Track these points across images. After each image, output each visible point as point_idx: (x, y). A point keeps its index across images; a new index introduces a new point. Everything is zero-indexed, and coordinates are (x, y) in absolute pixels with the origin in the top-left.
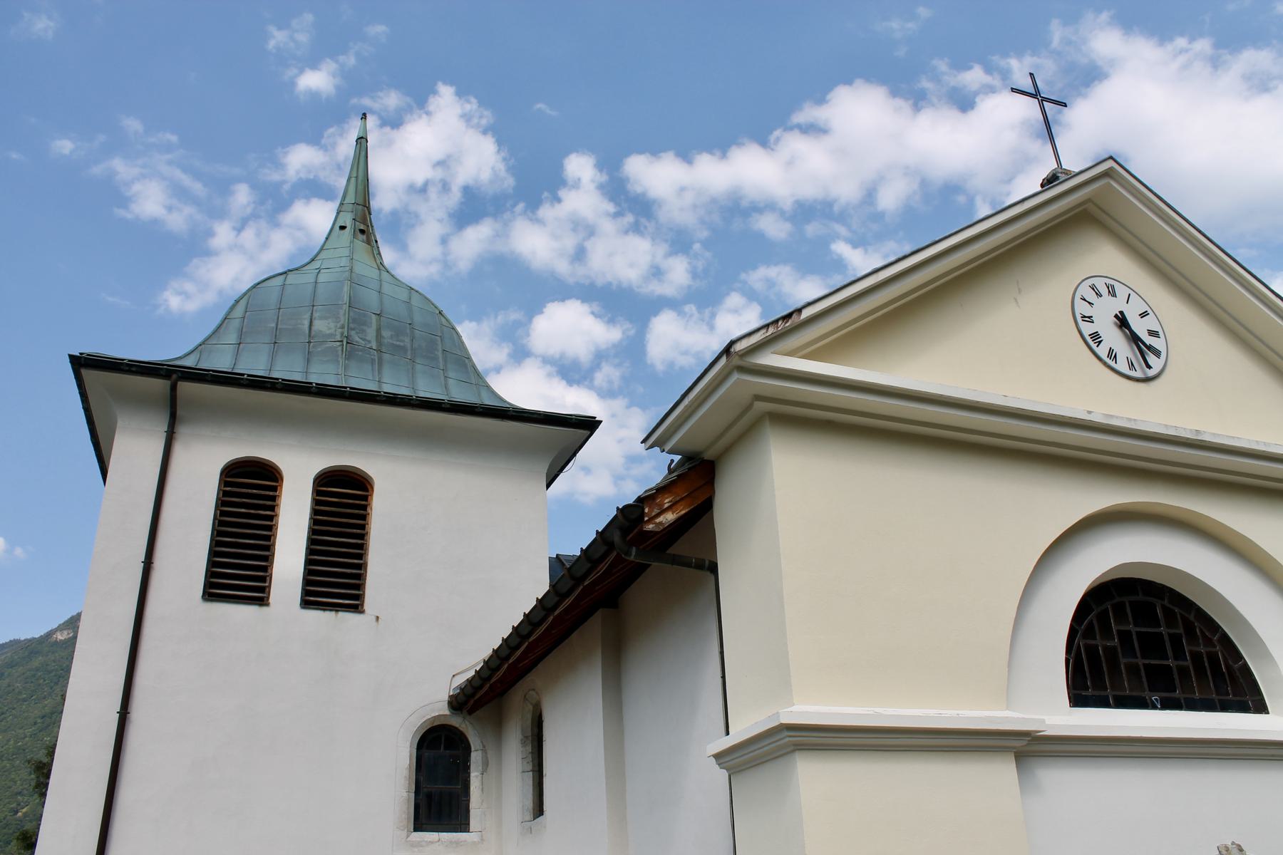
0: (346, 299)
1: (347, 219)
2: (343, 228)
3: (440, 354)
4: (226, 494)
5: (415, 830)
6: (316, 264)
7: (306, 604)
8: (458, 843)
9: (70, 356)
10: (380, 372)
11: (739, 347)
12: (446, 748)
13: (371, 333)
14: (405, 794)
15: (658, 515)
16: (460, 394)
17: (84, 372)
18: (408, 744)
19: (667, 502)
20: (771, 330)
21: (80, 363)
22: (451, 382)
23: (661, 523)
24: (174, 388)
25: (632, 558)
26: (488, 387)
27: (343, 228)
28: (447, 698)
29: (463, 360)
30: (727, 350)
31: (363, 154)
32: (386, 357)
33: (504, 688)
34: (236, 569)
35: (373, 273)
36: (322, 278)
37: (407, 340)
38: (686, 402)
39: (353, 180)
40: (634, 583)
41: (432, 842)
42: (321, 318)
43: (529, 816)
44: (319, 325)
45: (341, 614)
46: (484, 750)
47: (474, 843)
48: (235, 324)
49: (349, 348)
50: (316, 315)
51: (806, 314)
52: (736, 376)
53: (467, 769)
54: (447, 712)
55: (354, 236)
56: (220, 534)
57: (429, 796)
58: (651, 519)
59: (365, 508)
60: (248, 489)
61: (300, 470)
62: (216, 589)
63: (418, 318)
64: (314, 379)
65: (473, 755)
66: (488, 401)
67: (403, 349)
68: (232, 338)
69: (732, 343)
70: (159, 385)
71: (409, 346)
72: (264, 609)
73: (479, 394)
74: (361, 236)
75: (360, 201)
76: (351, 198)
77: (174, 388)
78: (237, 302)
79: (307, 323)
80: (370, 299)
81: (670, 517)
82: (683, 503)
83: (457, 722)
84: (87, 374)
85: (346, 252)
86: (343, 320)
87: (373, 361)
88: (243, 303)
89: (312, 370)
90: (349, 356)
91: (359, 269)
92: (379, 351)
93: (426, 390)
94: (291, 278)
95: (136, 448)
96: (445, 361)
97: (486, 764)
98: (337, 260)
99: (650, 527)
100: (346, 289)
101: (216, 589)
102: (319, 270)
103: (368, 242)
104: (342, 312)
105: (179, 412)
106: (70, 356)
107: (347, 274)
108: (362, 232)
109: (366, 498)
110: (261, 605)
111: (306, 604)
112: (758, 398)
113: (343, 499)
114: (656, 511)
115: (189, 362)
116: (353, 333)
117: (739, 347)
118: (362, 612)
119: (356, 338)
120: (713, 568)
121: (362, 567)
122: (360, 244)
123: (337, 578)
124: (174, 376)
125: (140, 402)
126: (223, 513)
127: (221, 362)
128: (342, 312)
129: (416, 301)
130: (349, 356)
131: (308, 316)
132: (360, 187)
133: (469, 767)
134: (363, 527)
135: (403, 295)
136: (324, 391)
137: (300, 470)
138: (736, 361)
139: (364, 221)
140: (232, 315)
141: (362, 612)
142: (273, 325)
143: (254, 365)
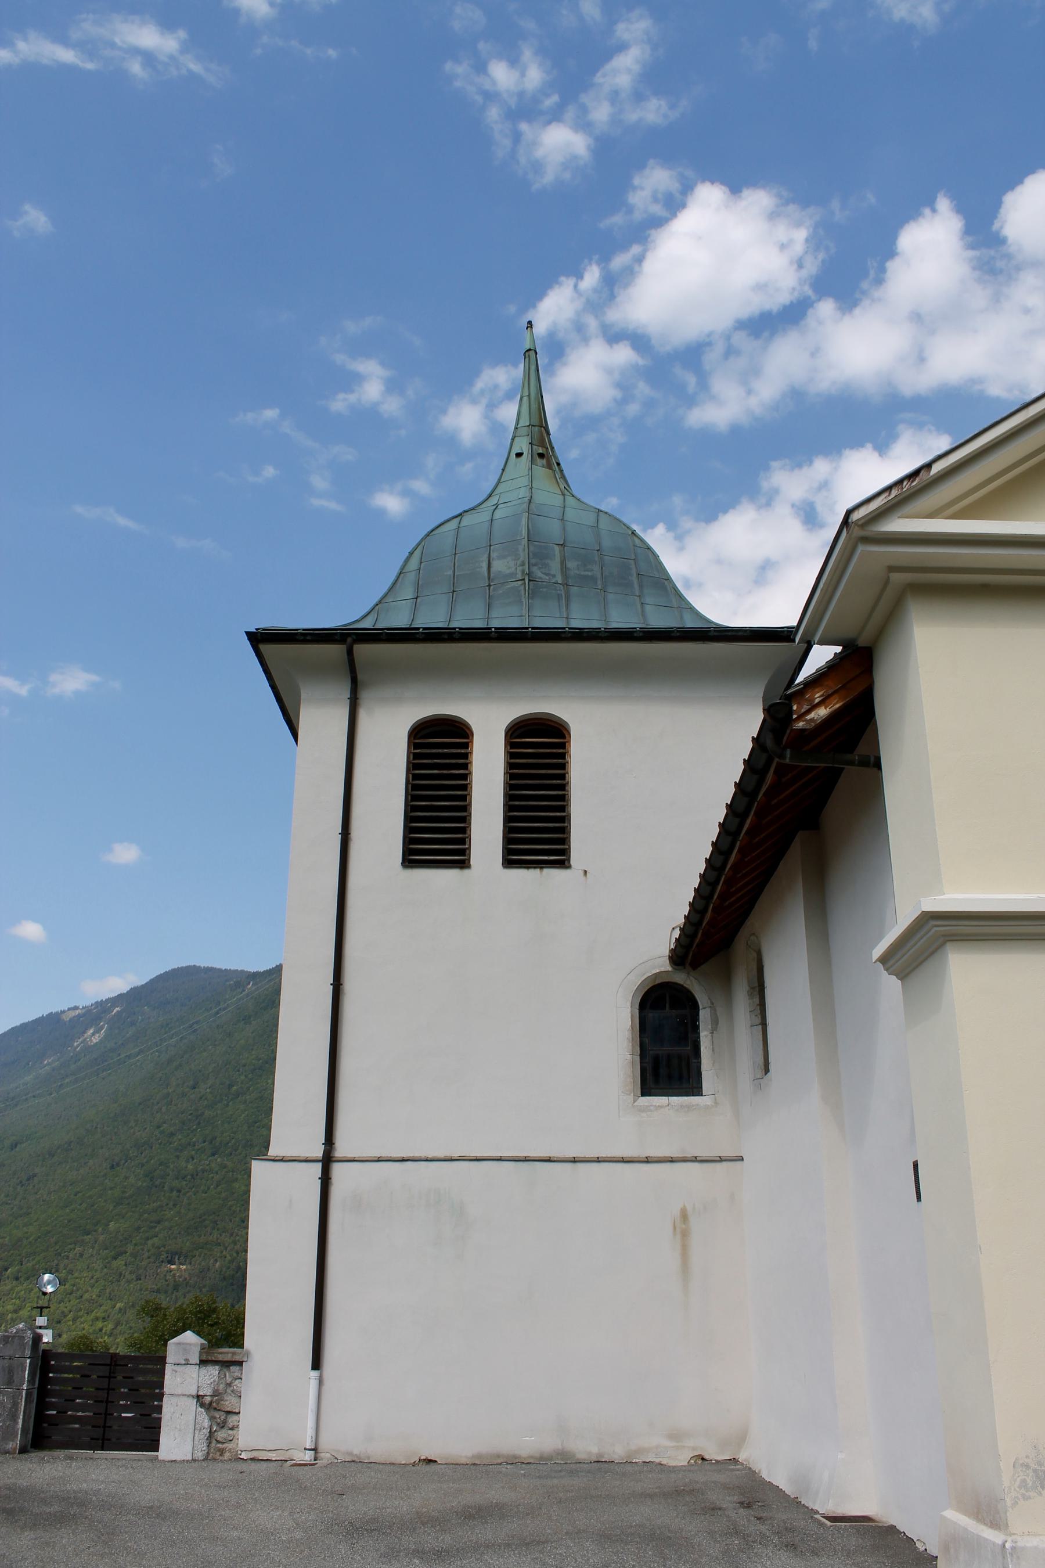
0: (524, 532)
1: (523, 444)
2: (519, 455)
3: (634, 579)
4: (416, 756)
5: (643, 1095)
6: (493, 500)
7: (509, 862)
8: (689, 1107)
9: (247, 633)
10: (567, 606)
11: (856, 516)
12: (672, 1007)
13: (555, 566)
14: (629, 1057)
15: (809, 711)
16: (658, 620)
17: (263, 647)
18: (629, 1004)
19: (818, 697)
20: (894, 492)
21: (258, 639)
22: (648, 608)
23: (812, 720)
24: (350, 652)
25: (787, 761)
26: (692, 609)
27: (519, 455)
28: (667, 953)
29: (660, 582)
30: (846, 522)
31: (533, 367)
32: (574, 590)
33: (720, 929)
34: (434, 834)
35: (557, 500)
36: (498, 514)
37: (596, 568)
38: (821, 585)
39: (525, 399)
40: (809, 791)
41: (661, 1107)
42: (499, 558)
43: (759, 1073)
44: (498, 566)
45: (545, 871)
46: (712, 1007)
47: (707, 1107)
48: (411, 577)
49: (532, 586)
50: (494, 555)
51: (936, 468)
52: (861, 548)
53: (696, 1028)
54: (669, 968)
55: (533, 461)
56: (415, 798)
57: (656, 1060)
58: (801, 717)
59: (563, 756)
60: (439, 749)
61: (487, 725)
62: (415, 854)
63: (607, 543)
64: (495, 624)
65: (702, 1013)
66: (690, 623)
67: (593, 579)
68: (408, 592)
69: (849, 513)
70: (335, 651)
71: (599, 575)
72: (466, 871)
73: (682, 617)
74: (538, 460)
75: (535, 422)
76: (525, 421)
77: (350, 652)
78: (411, 553)
79: (485, 565)
80: (552, 529)
81: (822, 712)
82: (836, 696)
83: (680, 978)
84: (265, 648)
85: (525, 481)
86: (523, 556)
87: (559, 597)
88: (418, 553)
89: (494, 614)
90: (532, 595)
91: (540, 498)
92: (566, 585)
93: (619, 620)
94: (466, 520)
95: (323, 718)
96: (641, 586)
97: (715, 1022)
98: (515, 491)
99: (801, 725)
100: (524, 521)
101: (415, 854)
102: (497, 506)
103: (549, 466)
104: (521, 548)
105: (360, 677)
106: (247, 633)
107: (525, 506)
108: (541, 456)
109: (563, 745)
110: (462, 868)
111: (509, 862)
112: (892, 569)
113: (539, 753)
114: (806, 707)
115: (367, 624)
116: (534, 569)
117: (856, 516)
118: (569, 867)
119: (538, 573)
120: (878, 765)
121: (566, 819)
122: (540, 470)
123: (539, 834)
124: (349, 640)
125: (319, 671)
126: (416, 777)
127: (398, 619)
128: (521, 548)
129: (604, 524)
130: (532, 595)
131: (485, 558)
132: (534, 406)
133: (698, 1027)
134: (563, 777)
135: (589, 519)
136: (505, 635)
137: (487, 725)
138: (857, 532)
139: (542, 443)
140: (408, 569)
141: (569, 867)
142: (450, 572)
143: (433, 618)
